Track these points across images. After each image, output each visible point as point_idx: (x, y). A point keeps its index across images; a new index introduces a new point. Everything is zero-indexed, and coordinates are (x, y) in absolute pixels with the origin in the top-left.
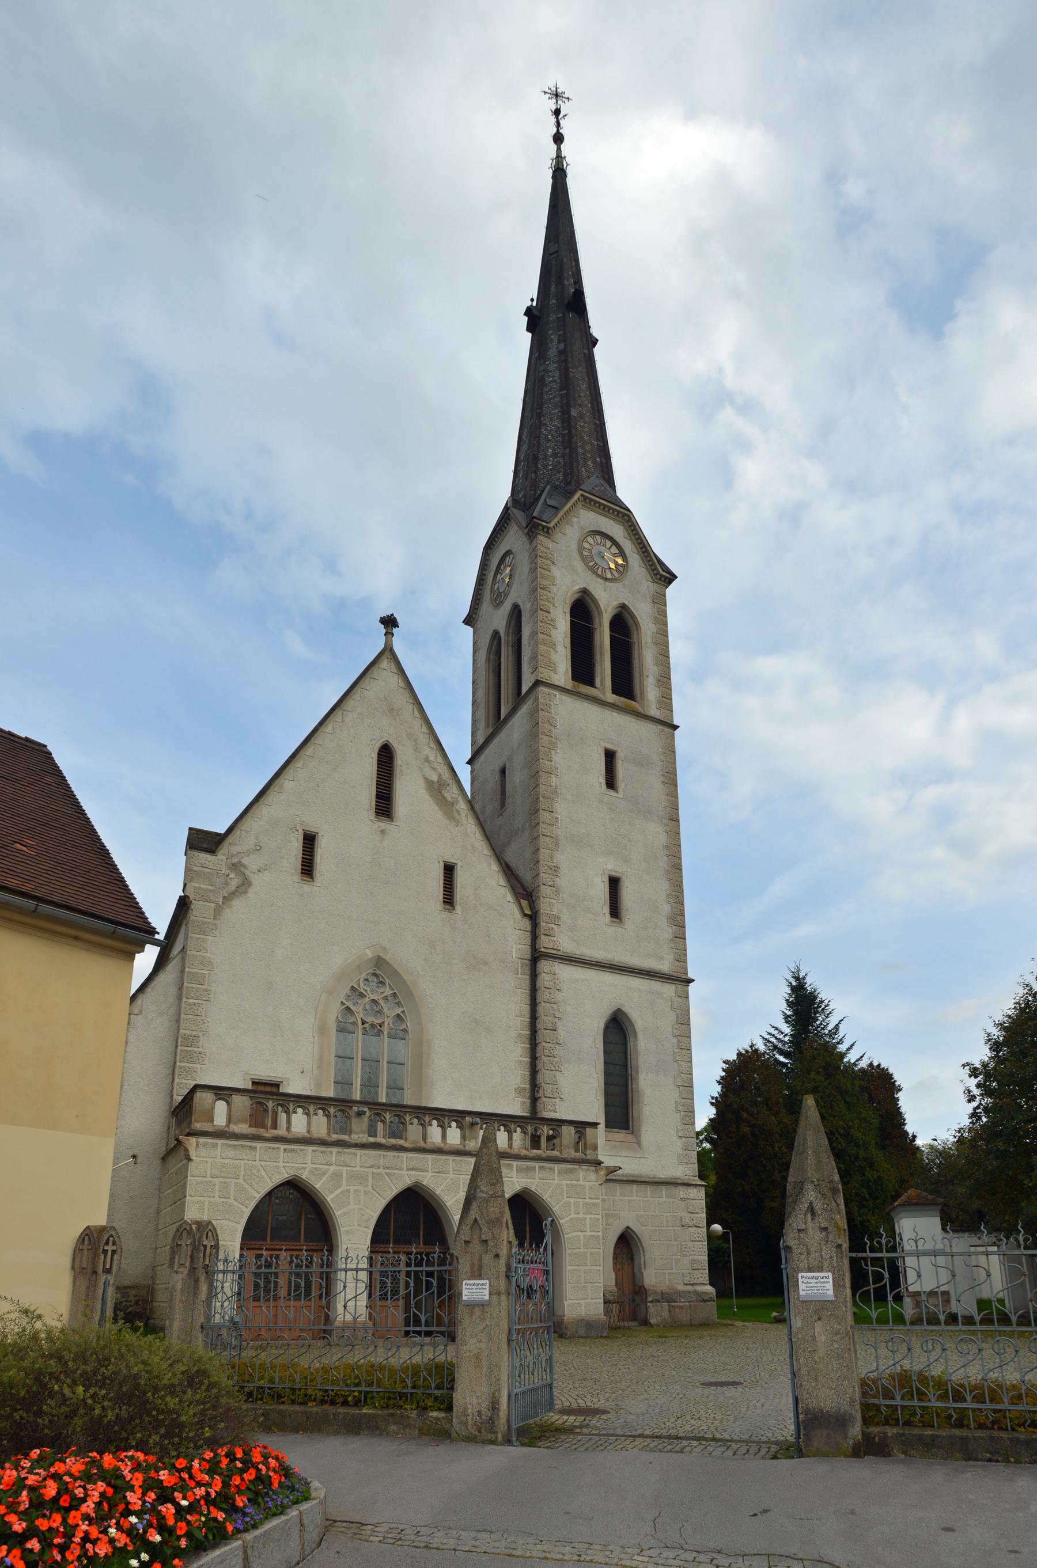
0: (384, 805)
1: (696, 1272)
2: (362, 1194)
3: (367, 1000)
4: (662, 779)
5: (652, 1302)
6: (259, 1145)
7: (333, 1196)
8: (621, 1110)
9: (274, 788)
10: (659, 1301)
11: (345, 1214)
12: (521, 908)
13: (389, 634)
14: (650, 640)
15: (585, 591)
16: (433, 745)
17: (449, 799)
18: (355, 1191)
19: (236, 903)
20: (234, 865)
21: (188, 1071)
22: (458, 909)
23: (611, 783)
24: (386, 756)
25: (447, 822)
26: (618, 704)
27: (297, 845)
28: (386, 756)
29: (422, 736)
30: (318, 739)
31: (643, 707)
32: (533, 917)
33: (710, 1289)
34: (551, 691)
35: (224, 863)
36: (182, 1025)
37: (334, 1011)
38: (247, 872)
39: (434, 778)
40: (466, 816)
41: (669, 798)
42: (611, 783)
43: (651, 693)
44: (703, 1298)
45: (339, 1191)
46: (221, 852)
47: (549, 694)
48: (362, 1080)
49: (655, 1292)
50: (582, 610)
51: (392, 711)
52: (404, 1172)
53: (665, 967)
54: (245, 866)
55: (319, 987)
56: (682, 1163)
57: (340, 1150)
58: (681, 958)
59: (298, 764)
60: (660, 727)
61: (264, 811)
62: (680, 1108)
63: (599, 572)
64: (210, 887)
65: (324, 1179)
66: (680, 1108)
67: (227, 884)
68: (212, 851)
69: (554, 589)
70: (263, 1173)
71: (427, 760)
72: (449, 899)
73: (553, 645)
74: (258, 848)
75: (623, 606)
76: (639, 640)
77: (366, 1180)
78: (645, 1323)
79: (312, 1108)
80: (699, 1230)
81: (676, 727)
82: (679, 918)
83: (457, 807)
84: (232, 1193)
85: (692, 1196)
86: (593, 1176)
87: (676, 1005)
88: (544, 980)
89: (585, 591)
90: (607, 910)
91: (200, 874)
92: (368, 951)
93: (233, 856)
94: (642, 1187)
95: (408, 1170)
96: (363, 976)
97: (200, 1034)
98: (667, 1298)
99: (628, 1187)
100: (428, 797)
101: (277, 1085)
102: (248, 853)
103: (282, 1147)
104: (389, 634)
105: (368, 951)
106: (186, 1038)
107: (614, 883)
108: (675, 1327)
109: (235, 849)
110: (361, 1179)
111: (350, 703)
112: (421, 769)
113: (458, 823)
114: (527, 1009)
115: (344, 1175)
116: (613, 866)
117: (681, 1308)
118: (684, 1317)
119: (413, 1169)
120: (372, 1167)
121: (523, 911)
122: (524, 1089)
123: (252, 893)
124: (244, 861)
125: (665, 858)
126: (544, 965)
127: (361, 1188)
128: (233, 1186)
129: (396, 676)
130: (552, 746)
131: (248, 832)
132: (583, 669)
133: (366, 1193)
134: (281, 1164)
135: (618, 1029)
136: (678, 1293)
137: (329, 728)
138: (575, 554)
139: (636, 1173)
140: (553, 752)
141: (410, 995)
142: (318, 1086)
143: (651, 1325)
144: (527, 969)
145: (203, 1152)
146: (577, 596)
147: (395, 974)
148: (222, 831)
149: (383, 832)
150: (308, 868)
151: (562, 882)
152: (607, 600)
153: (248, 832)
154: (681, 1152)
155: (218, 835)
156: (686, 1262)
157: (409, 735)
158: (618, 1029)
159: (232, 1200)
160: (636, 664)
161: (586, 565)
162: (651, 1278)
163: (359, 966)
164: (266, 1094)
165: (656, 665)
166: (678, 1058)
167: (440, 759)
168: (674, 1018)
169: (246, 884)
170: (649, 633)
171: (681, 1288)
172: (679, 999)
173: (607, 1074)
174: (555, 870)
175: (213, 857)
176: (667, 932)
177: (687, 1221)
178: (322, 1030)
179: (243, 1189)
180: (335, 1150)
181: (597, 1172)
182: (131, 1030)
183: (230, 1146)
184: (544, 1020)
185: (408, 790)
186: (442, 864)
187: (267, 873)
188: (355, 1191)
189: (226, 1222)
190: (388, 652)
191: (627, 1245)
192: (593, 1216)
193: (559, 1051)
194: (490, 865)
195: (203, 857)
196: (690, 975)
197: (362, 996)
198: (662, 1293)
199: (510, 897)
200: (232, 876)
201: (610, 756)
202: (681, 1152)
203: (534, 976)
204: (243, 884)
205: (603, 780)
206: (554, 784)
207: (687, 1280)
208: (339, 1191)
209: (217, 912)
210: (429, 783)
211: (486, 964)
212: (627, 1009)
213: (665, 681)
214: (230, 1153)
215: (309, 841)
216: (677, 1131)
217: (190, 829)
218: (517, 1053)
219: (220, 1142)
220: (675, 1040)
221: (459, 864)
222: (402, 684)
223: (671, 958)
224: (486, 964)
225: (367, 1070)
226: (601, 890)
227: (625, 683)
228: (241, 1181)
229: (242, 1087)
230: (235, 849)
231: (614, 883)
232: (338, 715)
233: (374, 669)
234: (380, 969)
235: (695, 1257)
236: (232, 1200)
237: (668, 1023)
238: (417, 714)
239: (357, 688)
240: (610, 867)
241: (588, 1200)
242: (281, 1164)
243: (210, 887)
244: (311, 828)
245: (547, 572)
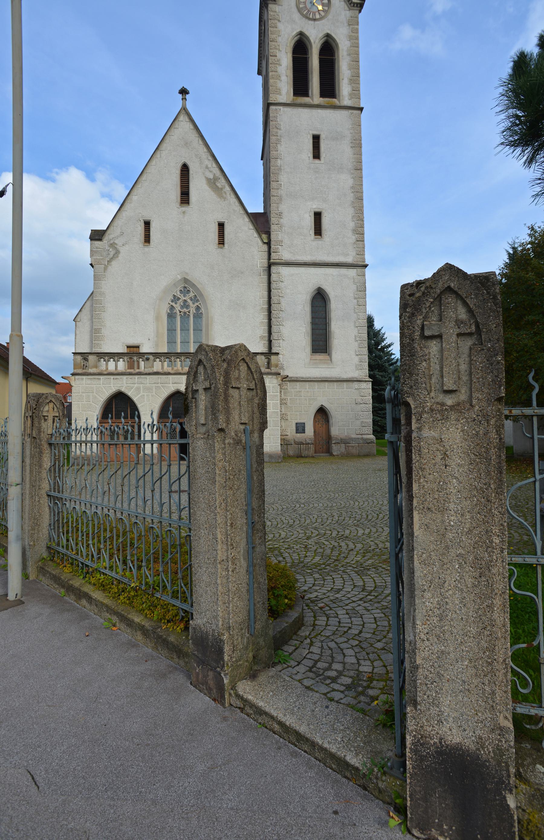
0: (185, 197)
1: (364, 428)
2: (150, 396)
3: (181, 300)
4: (351, 145)
5: (335, 444)
6: (101, 377)
7: (136, 398)
8: (321, 343)
9: (128, 201)
10: (339, 443)
11: (143, 406)
12: (262, 240)
13: (184, 99)
14: (345, 53)
15: (301, 34)
16: (210, 158)
17: (220, 187)
18: (147, 395)
19: (113, 263)
20: (111, 244)
21: (98, 344)
22: (226, 245)
23: (317, 155)
24: (185, 170)
25: (219, 199)
26: (322, 104)
27: (141, 228)
28: (185, 170)
29: (204, 154)
30: (148, 170)
31: (339, 101)
32: (269, 244)
33: (372, 437)
34: (279, 107)
35: (107, 245)
36: (94, 324)
37: (164, 310)
38: (118, 247)
39: (211, 176)
40: (230, 194)
41: (356, 156)
42: (317, 155)
43: (344, 88)
44: (368, 442)
45: (140, 395)
46: (105, 239)
47: (276, 110)
48: (181, 339)
49: (336, 439)
50: (300, 47)
51: (187, 144)
52: (171, 385)
53: (349, 260)
54: (116, 244)
55: (155, 297)
56: (357, 369)
57: (139, 376)
58: (361, 253)
59: (139, 186)
60: (350, 111)
61: (124, 214)
62: (358, 339)
63: (311, 16)
64: (101, 258)
65: (132, 390)
66: (358, 339)
67: (109, 254)
68: (100, 240)
69: (279, 39)
70: (104, 390)
71: (207, 167)
72: (221, 241)
73: (279, 77)
74: (122, 234)
75: (328, 36)
76: (338, 57)
77: (152, 390)
78: (331, 455)
79: (116, 358)
80: (367, 405)
81: (361, 109)
82: (359, 229)
83: (225, 190)
84: (91, 400)
85: (362, 387)
86: (275, 381)
87: (356, 281)
88: (274, 277)
89: (301, 34)
90: (312, 232)
91: (96, 252)
92: (178, 276)
93: (111, 240)
94: (331, 384)
95: (172, 383)
96: (179, 289)
97: (102, 327)
98: (345, 442)
99: (322, 384)
100: (208, 188)
101: (138, 347)
102: (117, 237)
103: (112, 377)
104: (184, 99)
105: (178, 276)
106: (96, 330)
107: (318, 216)
108: (348, 456)
109: (111, 237)
110: (149, 389)
111: (164, 145)
112: (204, 174)
113: (225, 199)
114: (266, 294)
115: (142, 388)
116: (316, 206)
117: (353, 447)
118: (354, 451)
119: (175, 383)
120: (155, 383)
121: (263, 241)
122: (264, 337)
123: (121, 256)
124: (116, 242)
125: (352, 194)
126: (274, 269)
127: (150, 394)
128: (91, 397)
129: (188, 123)
130: (278, 141)
131: (117, 227)
132: (300, 87)
133: (152, 396)
134: (112, 385)
135: (320, 299)
136: (352, 439)
137: (153, 162)
138: (295, 10)
139: (329, 376)
140: (279, 145)
141: (201, 295)
142: (157, 345)
143: (334, 456)
144: (266, 273)
145: (78, 382)
146: (296, 39)
147: (194, 286)
148: (105, 229)
149: (184, 212)
150: (147, 239)
151: (284, 221)
152: (315, 36)
153: (117, 227)
154: (357, 363)
155: (104, 230)
156: (358, 423)
157: (196, 156)
158: (320, 299)
159: (91, 403)
160: (337, 74)
161: (302, 14)
162: (335, 431)
163: (174, 284)
164: (133, 353)
165: (350, 69)
166: (357, 311)
167: (214, 165)
168: (355, 288)
169: (117, 252)
170: (345, 48)
171: (354, 436)
172: (359, 277)
173: (313, 323)
174: (280, 215)
175: (101, 242)
176: (352, 238)
177: (359, 399)
178: (158, 318)
179: (96, 397)
180: (136, 377)
181: (277, 378)
182: (77, 328)
183: (89, 379)
184: (274, 299)
185: (198, 186)
186: (217, 224)
187: (127, 246)
188: (147, 395)
189: (90, 412)
190: (184, 109)
191: (322, 412)
192: (274, 402)
193: (282, 314)
194: (244, 219)
195: (97, 243)
196: (367, 263)
197: (179, 299)
198: (341, 439)
199: (256, 235)
200: (111, 250)
201: (316, 139)
202: (357, 363)
203: (269, 275)
204: (116, 253)
205: (311, 155)
206: (279, 165)
207: (358, 432)
208: (140, 395)
209: (105, 269)
210: (208, 180)
211: (242, 273)
212: (324, 287)
213: (355, 79)
214: (89, 382)
215: (147, 224)
216: (356, 351)
217: (92, 230)
218: (262, 318)
219: (84, 377)
220: (356, 301)
221: (226, 221)
222: (192, 127)
223: (354, 253)
224: (242, 273)
225: (184, 335)
226: (309, 221)
227: (329, 89)
228: (95, 394)
229: (88, 352)
230: (111, 237)
231: (318, 216)
232: (158, 154)
233: (176, 122)
234: (187, 286)
235: (364, 420)
236: (91, 403)
237: (351, 290)
238: (201, 142)
239: (167, 136)
240: (314, 207)
241: (271, 393)
242: (112, 385)
243: (101, 258)
244: (147, 219)
245: (275, 29)
